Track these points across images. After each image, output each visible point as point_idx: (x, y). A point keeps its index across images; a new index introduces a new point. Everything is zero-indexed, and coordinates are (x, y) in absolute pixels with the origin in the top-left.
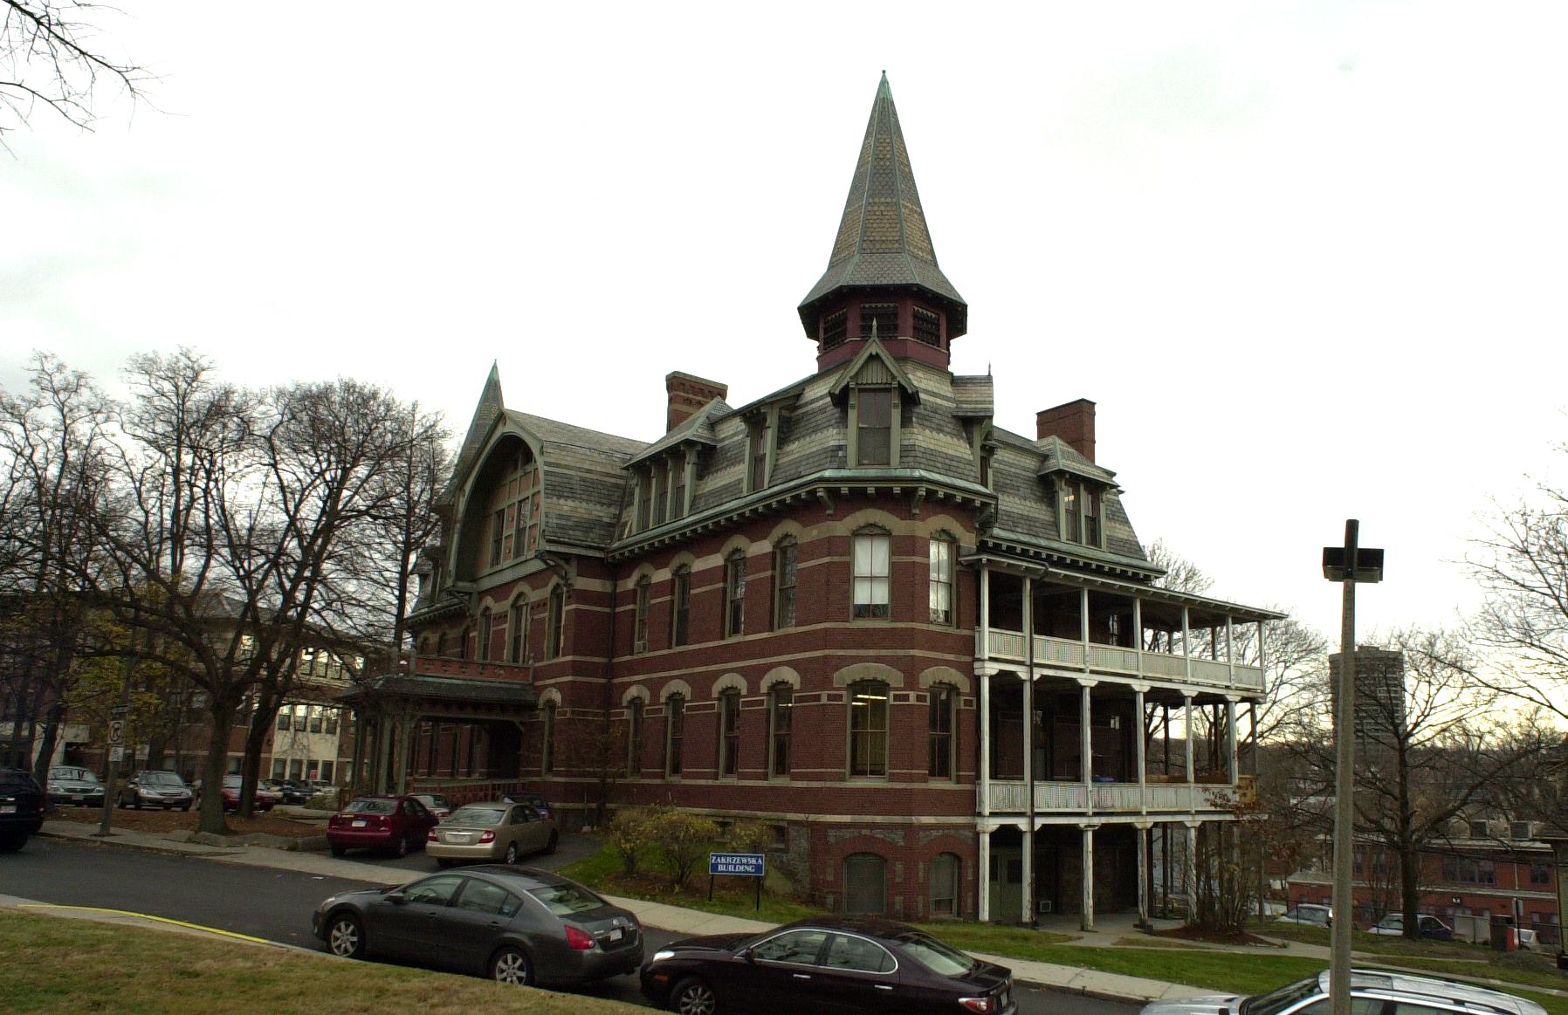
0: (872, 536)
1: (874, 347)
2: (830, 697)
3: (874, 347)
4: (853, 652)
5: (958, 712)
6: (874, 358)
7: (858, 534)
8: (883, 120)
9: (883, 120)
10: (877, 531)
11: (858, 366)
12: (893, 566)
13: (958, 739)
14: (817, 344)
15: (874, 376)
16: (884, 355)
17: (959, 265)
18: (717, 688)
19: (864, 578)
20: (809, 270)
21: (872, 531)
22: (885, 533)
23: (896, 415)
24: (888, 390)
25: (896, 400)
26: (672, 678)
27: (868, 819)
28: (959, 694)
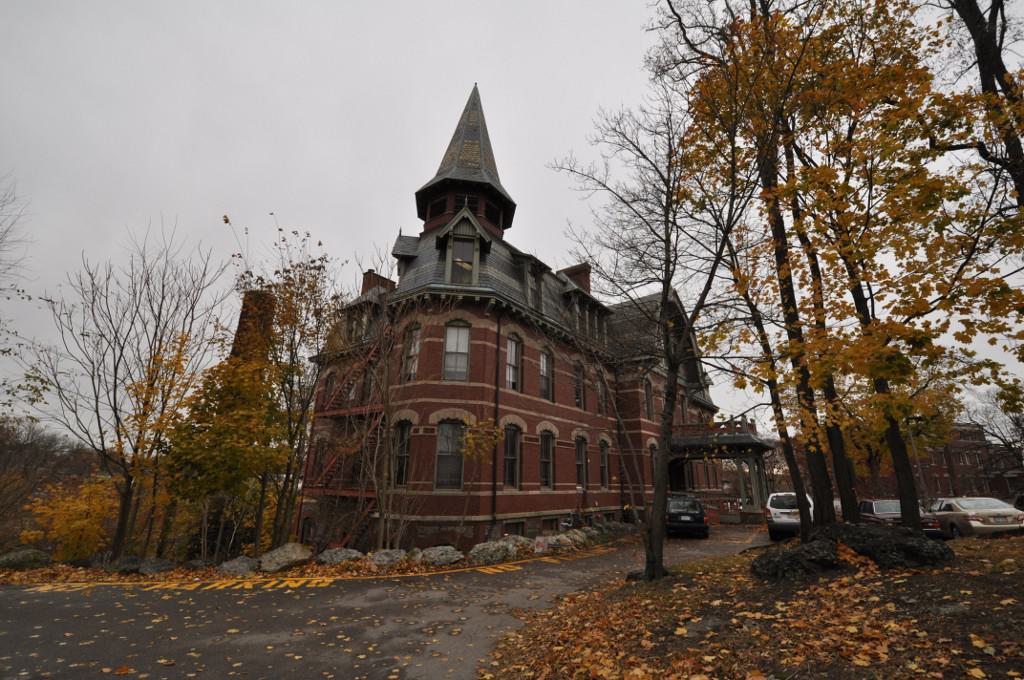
0: (458, 327)
1: (466, 213)
2: (426, 430)
3: (466, 213)
4: (445, 401)
5: (554, 448)
6: (465, 220)
7: (449, 325)
8: (474, 104)
9: (474, 104)
10: (461, 324)
11: (457, 221)
12: (472, 346)
13: (521, 462)
14: (423, 222)
15: (464, 231)
16: (472, 220)
17: (510, 182)
18: (574, 433)
19: (452, 353)
20: (427, 172)
21: (455, 323)
22: (468, 326)
23: (477, 255)
24: (472, 241)
25: (477, 246)
26: (545, 419)
27: (445, 518)
28: (522, 433)
